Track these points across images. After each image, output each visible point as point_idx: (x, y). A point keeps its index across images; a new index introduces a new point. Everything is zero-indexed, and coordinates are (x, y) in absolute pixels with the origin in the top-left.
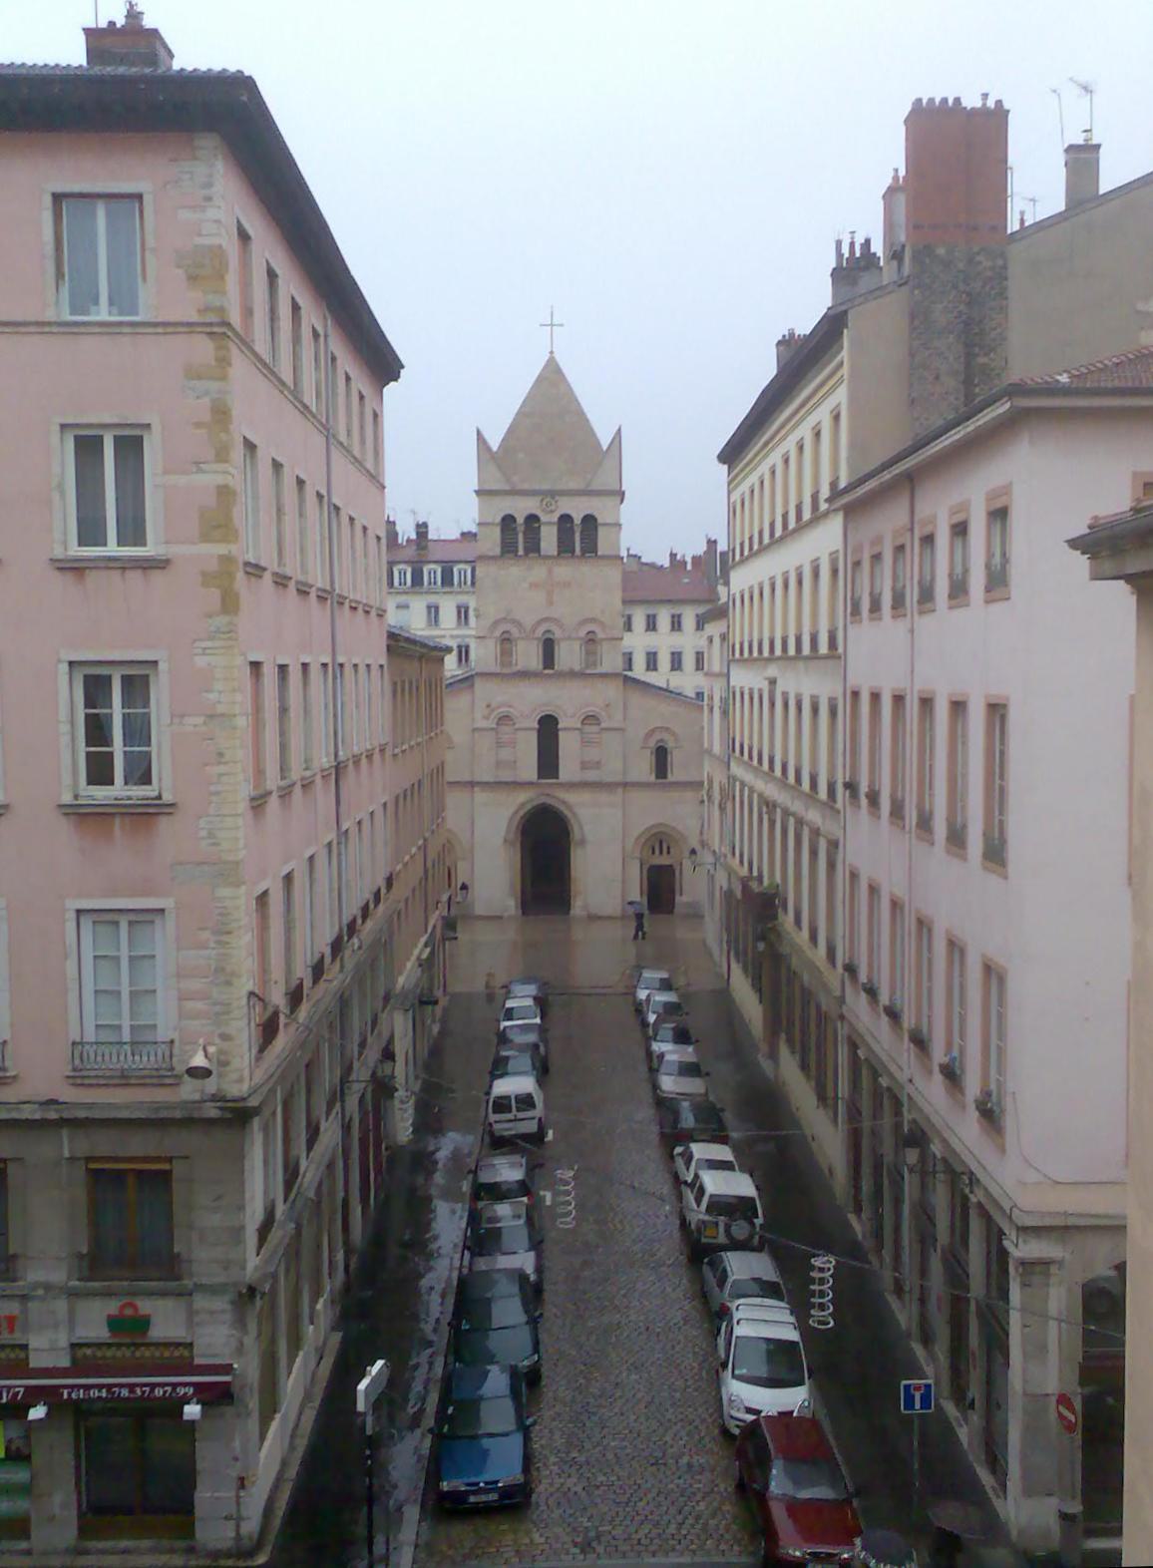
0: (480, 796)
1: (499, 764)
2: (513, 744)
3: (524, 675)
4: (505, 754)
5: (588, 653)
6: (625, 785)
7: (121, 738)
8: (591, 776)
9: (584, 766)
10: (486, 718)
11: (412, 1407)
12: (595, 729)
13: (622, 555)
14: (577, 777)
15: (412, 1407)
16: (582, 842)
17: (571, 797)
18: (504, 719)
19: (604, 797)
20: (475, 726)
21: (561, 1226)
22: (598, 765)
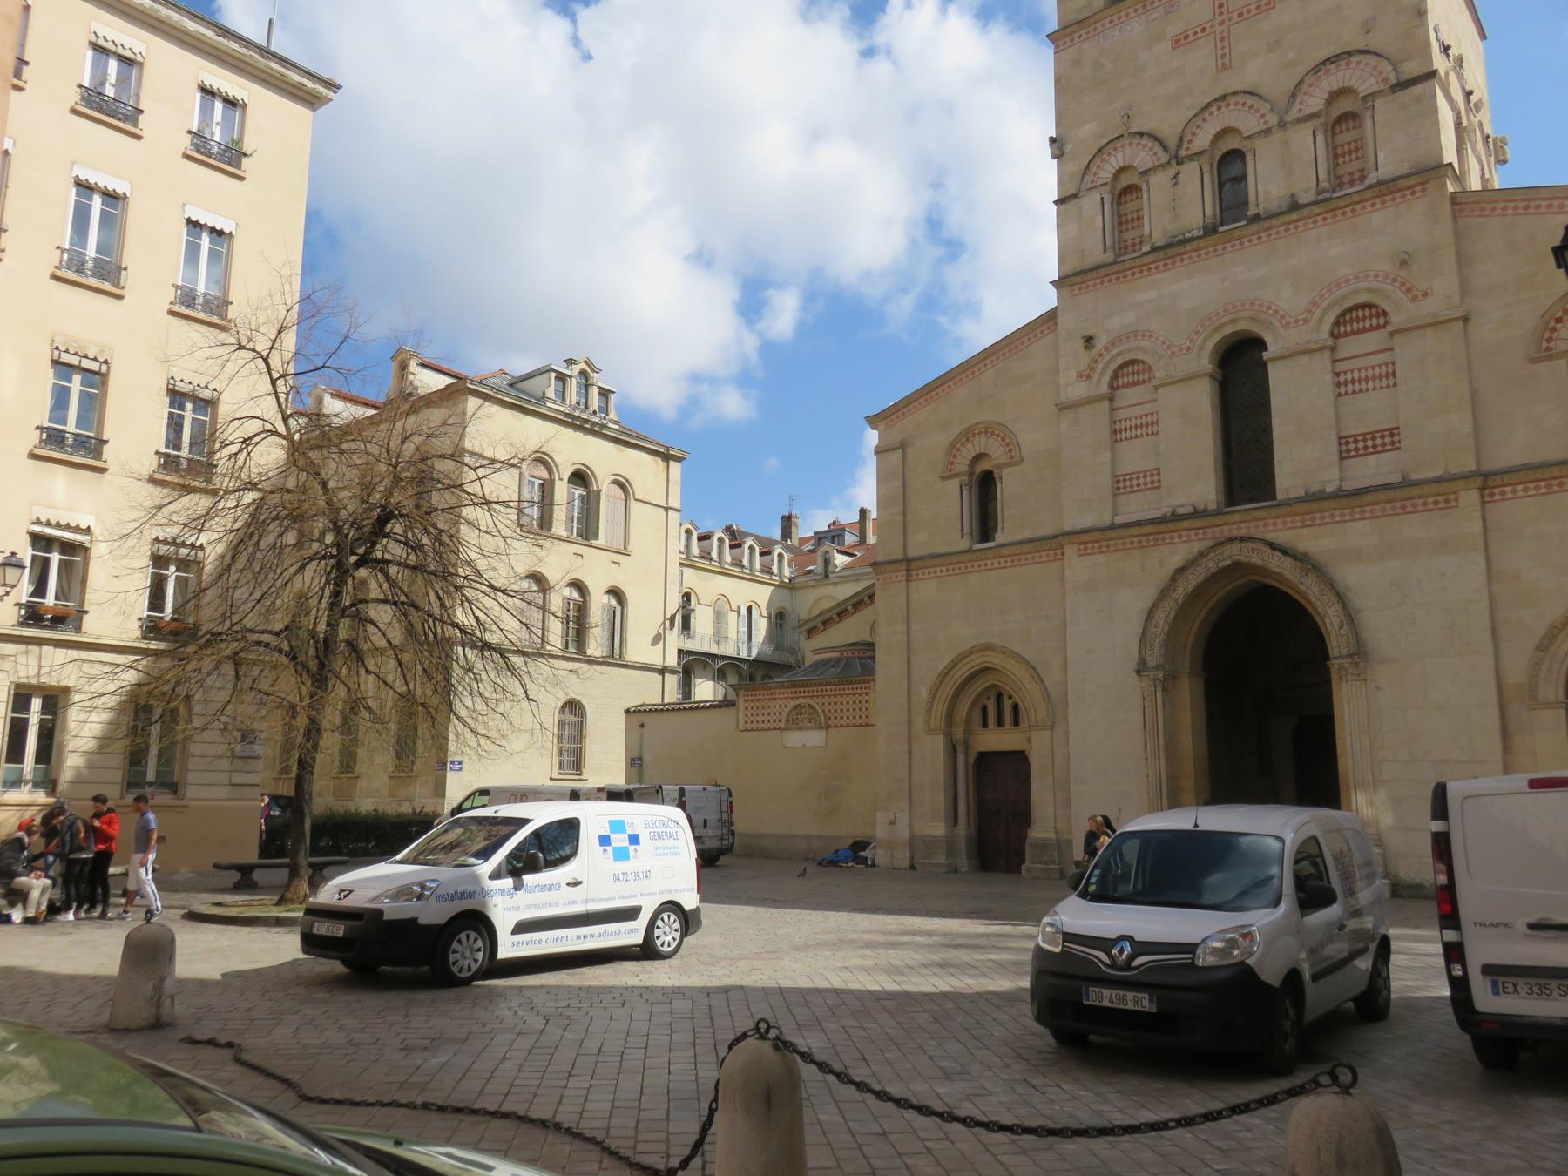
0: (1078, 567)
1: (1120, 484)
2: (1150, 426)
3: (1173, 248)
4: (1134, 457)
5: (1335, 155)
6: (1487, 481)
7: (513, 838)
8: (1371, 470)
9: (1349, 447)
10: (1085, 376)
11: (147, 875)
12: (1373, 340)
13: (1447, 160)
14: (1330, 478)
15: (147, 875)
16: (1360, 654)
17: (1316, 540)
18: (1129, 371)
19: (1414, 527)
20: (1063, 398)
21: (1124, 956)
22: (1389, 438)
